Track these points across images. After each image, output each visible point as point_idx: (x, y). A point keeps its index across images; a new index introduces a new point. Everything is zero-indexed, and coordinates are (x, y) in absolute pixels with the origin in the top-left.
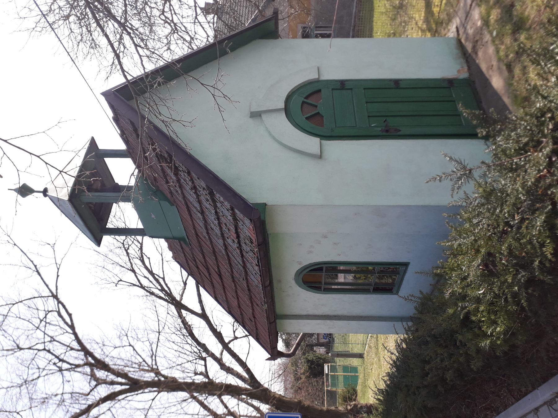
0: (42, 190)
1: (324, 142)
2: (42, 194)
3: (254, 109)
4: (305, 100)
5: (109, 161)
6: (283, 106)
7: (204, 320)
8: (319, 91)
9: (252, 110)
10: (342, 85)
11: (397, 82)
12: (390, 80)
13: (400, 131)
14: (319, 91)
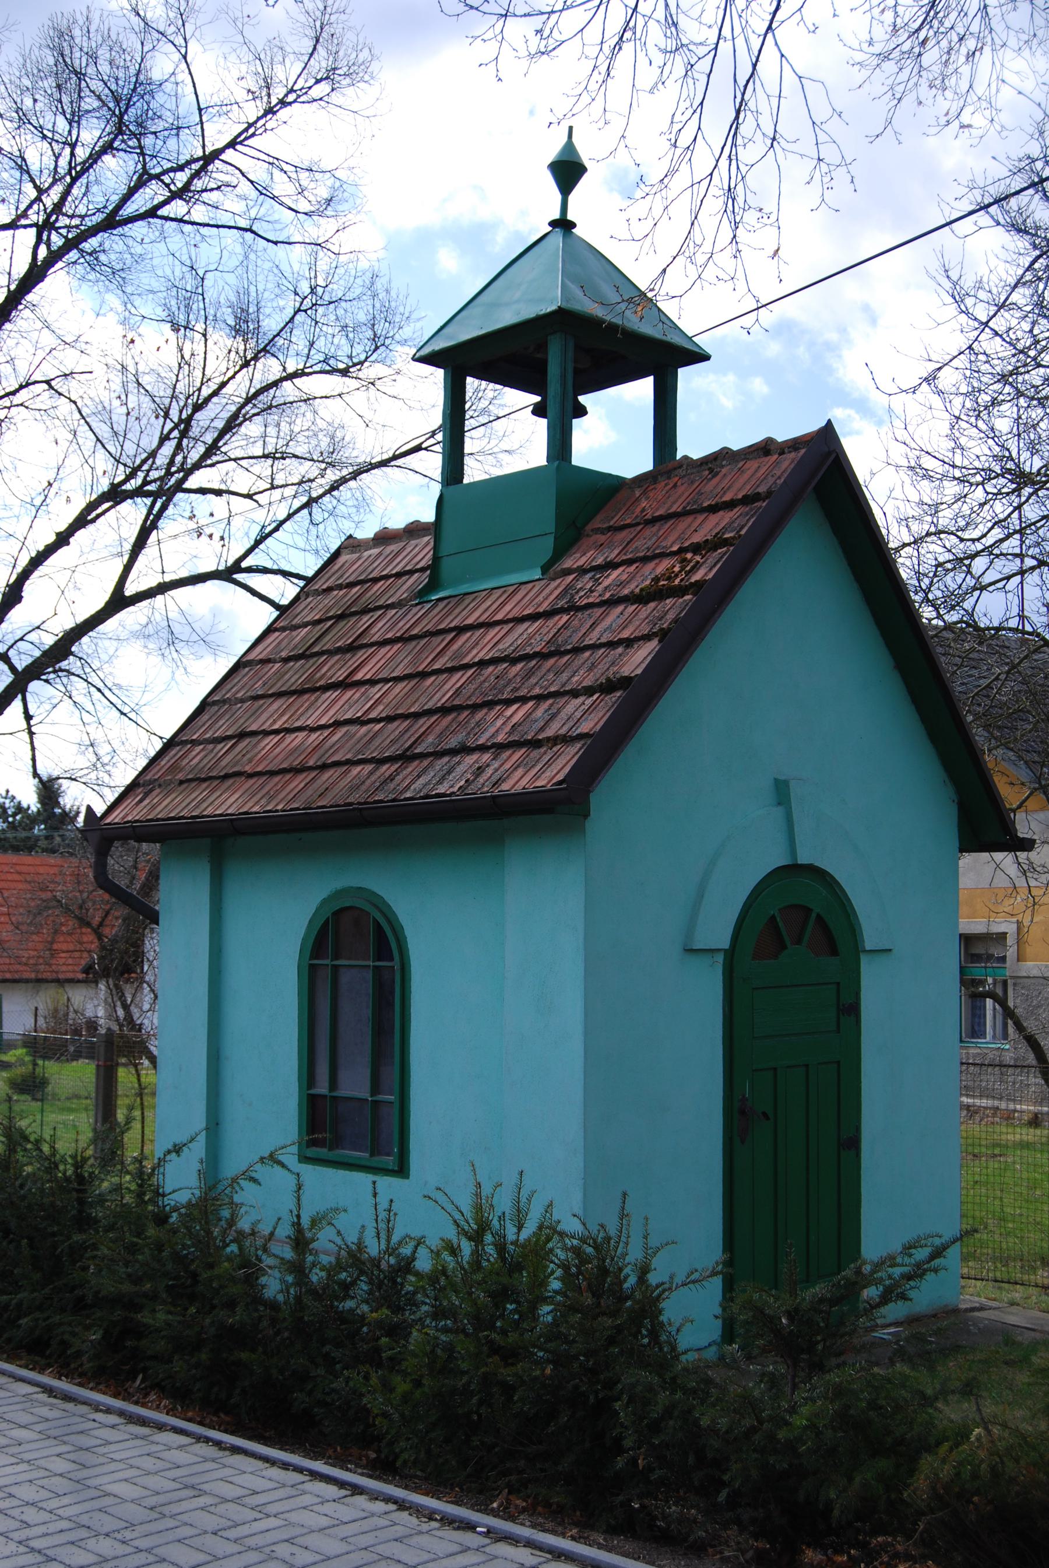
0: (570, 217)
1: (720, 958)
2: (556, 215)
3: (796, 791)
4: (814, 915)
5: (643, 389)
6: (803, 859)
7: (108, 604)
8: (834, 951)
9: (792, 784)
10: (851, 1010)
11: (853, 1143)
12: (858, 1129)
13: (743, 1142)
14: (834, 951)
